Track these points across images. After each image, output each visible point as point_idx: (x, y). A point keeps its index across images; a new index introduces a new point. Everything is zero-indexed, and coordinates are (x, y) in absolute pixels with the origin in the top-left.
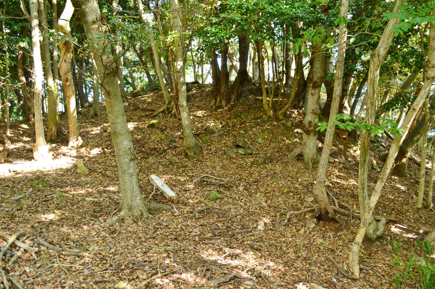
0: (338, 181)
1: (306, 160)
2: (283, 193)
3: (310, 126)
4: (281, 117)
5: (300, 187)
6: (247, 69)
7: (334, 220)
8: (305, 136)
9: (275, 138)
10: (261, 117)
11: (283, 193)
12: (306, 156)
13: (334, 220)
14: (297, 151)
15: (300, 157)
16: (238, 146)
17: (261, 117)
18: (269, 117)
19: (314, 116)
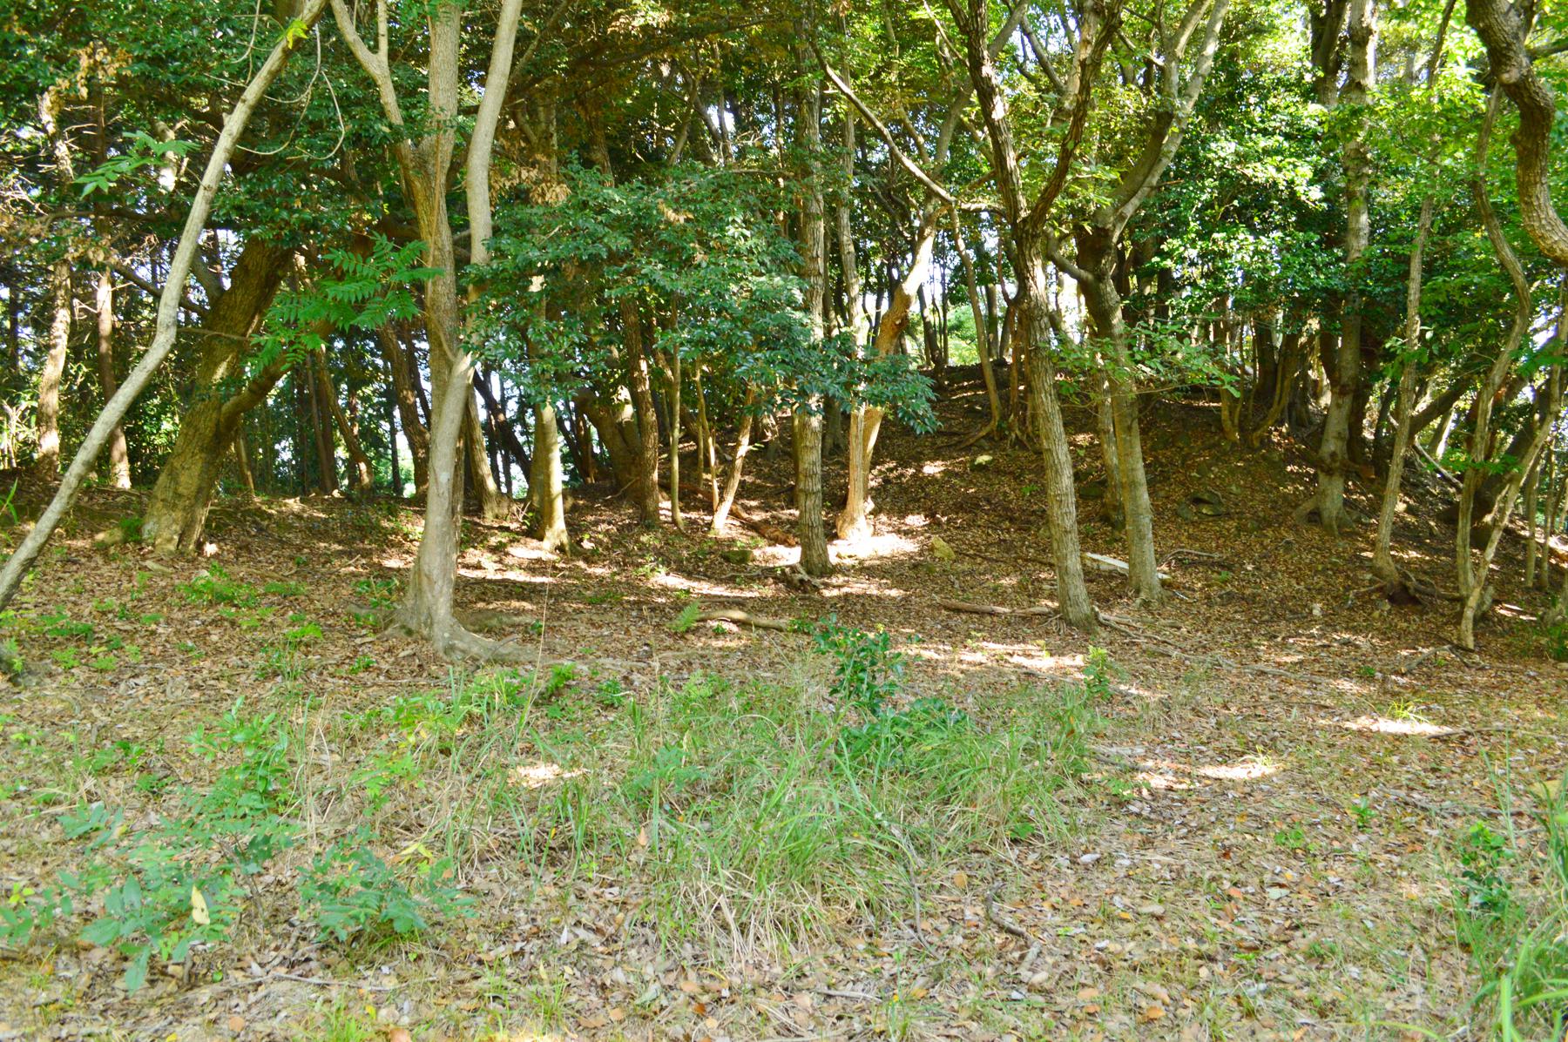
0: (927, 654)
1: (1326, 521)
2: (1317, 572)
3: (1334, 461)
4: (1257, 444)
5: (1340, 562)
6: (1083, 298)
7: (1415, 601)
8: (1322, 477)
9: (1258, 484)
10: (1217, 445)
11: (1317, 572)
12: (1325, 514)
13: (1415, 601)
14: (1308, 506)
15: (1315, 517)
16: (1198, 501)
17: (1217, 445)
18: (1234, 444)
19: (1340, 444)
